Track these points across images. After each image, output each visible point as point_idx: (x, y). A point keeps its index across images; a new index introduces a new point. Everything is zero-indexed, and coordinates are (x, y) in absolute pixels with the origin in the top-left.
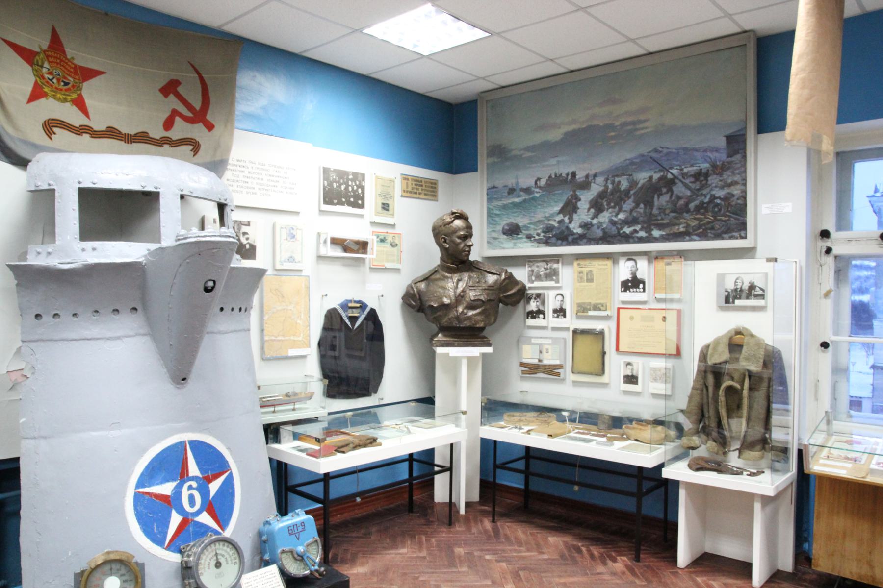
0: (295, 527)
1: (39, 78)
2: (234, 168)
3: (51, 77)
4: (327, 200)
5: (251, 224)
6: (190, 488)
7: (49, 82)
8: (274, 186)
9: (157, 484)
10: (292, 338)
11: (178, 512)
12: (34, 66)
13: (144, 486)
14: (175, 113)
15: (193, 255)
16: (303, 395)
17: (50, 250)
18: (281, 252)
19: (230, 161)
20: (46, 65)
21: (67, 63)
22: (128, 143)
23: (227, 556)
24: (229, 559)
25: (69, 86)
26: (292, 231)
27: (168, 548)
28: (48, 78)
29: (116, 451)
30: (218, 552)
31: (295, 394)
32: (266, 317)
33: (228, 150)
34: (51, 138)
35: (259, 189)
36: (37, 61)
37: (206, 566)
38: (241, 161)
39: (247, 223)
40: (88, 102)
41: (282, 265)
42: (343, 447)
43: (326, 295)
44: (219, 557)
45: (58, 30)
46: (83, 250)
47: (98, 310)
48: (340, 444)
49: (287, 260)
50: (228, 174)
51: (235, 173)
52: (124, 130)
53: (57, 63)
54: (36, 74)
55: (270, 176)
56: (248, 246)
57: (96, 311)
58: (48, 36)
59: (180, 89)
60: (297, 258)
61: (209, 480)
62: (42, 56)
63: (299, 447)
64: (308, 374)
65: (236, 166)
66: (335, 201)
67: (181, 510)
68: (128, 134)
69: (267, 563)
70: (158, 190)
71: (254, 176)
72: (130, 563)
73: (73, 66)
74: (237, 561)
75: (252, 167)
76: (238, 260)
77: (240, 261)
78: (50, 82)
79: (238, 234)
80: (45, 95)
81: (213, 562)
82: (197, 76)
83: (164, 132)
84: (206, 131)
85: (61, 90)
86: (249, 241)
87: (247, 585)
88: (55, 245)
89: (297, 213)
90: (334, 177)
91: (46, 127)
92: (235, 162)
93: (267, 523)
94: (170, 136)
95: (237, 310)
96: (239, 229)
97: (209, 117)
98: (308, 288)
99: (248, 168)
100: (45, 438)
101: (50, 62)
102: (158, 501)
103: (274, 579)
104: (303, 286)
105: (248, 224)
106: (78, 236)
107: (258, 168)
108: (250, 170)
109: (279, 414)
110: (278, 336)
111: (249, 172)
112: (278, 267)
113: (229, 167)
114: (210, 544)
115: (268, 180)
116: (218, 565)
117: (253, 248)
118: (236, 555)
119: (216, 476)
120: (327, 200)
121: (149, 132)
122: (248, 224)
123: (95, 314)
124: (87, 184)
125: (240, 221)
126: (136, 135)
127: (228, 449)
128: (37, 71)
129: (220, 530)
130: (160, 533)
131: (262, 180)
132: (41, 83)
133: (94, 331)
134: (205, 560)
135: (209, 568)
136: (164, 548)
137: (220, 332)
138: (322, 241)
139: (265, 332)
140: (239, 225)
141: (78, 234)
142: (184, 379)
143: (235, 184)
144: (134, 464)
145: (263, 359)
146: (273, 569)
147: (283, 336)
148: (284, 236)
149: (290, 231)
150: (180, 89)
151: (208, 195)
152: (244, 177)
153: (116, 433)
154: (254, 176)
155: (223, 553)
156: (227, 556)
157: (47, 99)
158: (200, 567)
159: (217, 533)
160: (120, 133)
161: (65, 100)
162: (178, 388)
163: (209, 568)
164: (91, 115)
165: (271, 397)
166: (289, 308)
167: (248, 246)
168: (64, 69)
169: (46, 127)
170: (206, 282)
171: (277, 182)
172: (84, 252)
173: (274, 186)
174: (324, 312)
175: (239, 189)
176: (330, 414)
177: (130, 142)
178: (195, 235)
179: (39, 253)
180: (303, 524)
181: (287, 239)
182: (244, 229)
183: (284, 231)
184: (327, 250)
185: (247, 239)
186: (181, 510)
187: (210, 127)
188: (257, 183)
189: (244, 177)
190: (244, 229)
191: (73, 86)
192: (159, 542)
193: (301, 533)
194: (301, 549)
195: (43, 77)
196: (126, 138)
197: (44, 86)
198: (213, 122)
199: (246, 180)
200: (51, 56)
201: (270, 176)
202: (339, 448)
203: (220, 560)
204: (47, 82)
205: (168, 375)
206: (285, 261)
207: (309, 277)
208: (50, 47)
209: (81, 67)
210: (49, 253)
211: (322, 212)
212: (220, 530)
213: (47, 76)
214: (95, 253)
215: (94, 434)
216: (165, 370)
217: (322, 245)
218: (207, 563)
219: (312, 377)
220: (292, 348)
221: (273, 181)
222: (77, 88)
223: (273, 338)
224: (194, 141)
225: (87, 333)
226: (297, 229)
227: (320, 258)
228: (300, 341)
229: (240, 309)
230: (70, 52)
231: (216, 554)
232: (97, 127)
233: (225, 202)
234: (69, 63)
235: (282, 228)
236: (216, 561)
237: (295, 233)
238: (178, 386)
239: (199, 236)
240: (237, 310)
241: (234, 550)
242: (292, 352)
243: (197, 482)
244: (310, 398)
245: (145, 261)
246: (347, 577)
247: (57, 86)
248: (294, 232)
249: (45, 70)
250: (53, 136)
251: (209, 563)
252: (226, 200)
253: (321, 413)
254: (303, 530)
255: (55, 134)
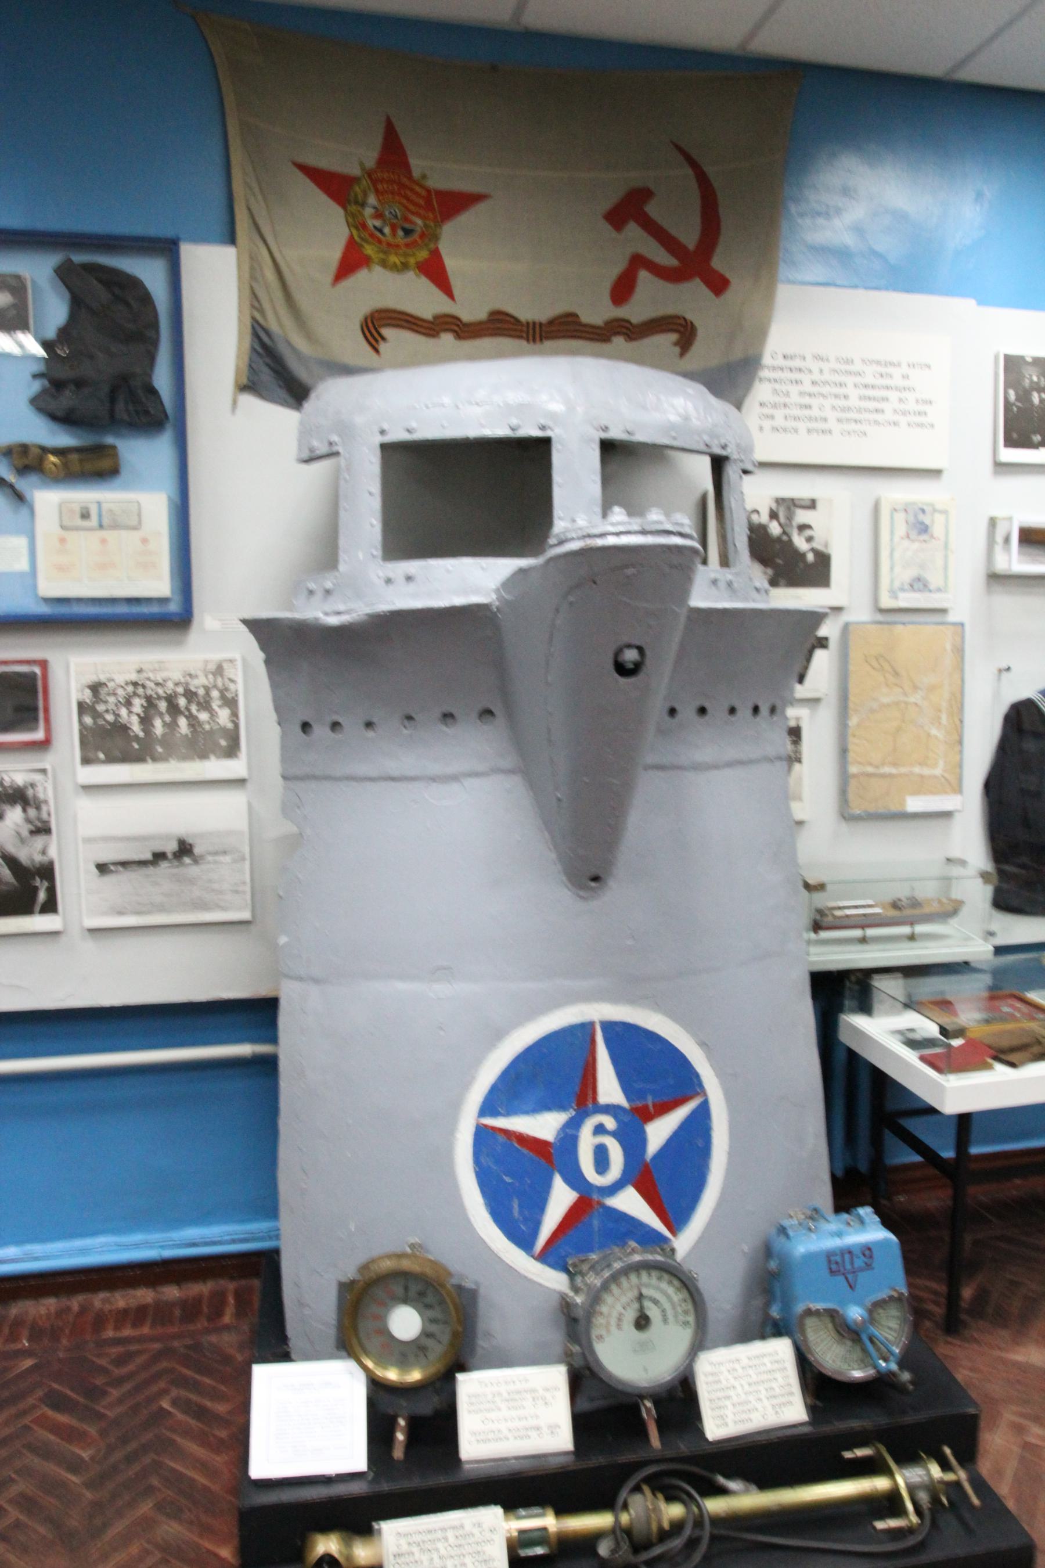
0: (847, 1257)
1: (357, 228)
2: (778, 375)
3: (378, 223)
4: (1015, 436)
5: (819, 505)
6: (600, 1129)
7: (377, 233)
8: (877, 411)
9: (526, 1112)
10: (917, 770)
11: (567, 1181)
12: (349, 208)
13: (495, 1114)
14: (638, 262)
15: (578, 586)
16: (935, 907)
17: (329, 585)
18: (892, 568)
19: (767, 360)
20: (372, 200)
21: (412, 190)
22: (534, 341)
23: (667, 1305)
24: (670, 1313)
25: (416, 236)
26: (921, 517)
27: (543, 1257)
28: (375, 227)
29: (441, 1028)
30: (645, 1291)
31: (915, 903)
32: (853, 721)
33: (761, 333)
34: (377, 351)
35: (839, 420)
36: (356, 196)
37: (613, 1321)
38: (792, 357)
39: (808, 503)
40: (451, 264)
41: (896, 598)
42: (1013, 1050)
43: (1008, 669)
44: (647, 1304)
45: (394, 120)
46: (389, 581)
47: (414, 715)
48: (1005, 1043)
49: (907, 587)
50: (761, 391)
51: (777, 386)
52: (526, 314)
53: (392, 193)
54: (350, 220)
55: (866, 386)
56: (810, 557)
57: (409, 718)
58: (378, 140)
59: (652, 209)
60: (934, 579)
61: (646, 1115)
62: (365, 183)
63: (912, 1030)
64: (956, 853)
65: (782, 369)
66: (1037, 438)
67: (575, 1179)
68: (534, 323)
69: (777, 1329)
70: (548, 433)
71: (825, 390)
72: (443, 1286)
73: (424, 193)
74: (691, 1319)
75: (821, 371)
76: (757, 590)
77: (767, 592)
78: (378, 234)
79: (788, 530)
80: (365, 262)
81: (631, 1315)
82: (690, 172)
83: (612, 307)
84: (709, 294)
85: (398, 246)
86: (815, 545)
87: (711, 1379)
88: (337, 574)
89: (936, 473)
90: (1035, 379)
91: (370, 332)
92: (780, 362)
93: (783, 1231)
94: (627, 316)
95: (745, 712)
96: (790, 518)
97: (718, 263)
98: (959, 651)
99: (810, 371)
100: (316, 981)
101: (377, 191)
102: (525, 1151)
103: (778, 1375)
104: (948, 647)
105: (812, 505)
106: (378, 552)
107: (835, 371)
108: (816, 376)
109: (874, 947)
110: (883, 764)
111: (814, 383)
112: (886, 602)
113: (764, 373)
114: (626, 1271)
115: (862, 398)
116: (642, 1322)
117: (823, 560)
118: (690, 1306)
119: (664, 1108)
120: (1015, 436)
121: (579, 313)
122: (812, 505)
123: (406, 722)
124: (398, 435)
125: (793, 500)
126: (551, 322)
127: (703, 1044)
128: (353, 215)
129: (666, 1232)
130: (526, 1220)
131: (846, 397)
132: (360, 237)
133: (406, 762)
134: (613, 1307)
135: (619, 1326)
136: (533, 1256)
137: (698, 767)
138: (999, 538)
139: (851, 756)
140: (789, 509)
141: (379, 546)
142: (596, 879)
143: (779, 414)
144: (477, 1062)
145: (844, 818)
146: (782, 1348)
147: (895, 764)
148: (901, 529)
149: (916, 516)
150: (652, 209)
151: (675, 438)
152: (801, 394)
153: (441, 989)
154: (825, 390)
155: (657, 1295)
156: (667, 1305)
157: (370, 270)
158: (599, 1321)
159: (649, 1238)
160: (517, 321)
161: (405, 267)
162: (581, 897)
163: (619, 1326)
164: (456, 292)
165: (856, 907)
166: (912, 699)
167: (810, 557)
168: (405, 202)
169: (370, 332)
170: (618, 652)
171: (885, 399)
172: (391, 587)
173: (877, 411)
174: (1003, 709)
175: (791, 424)
176: (999, 950)
177: (531, 338)
178: (580, 533)
179: (311, 592)
180: (867, 1253)
181: (908, 536)
182: (802, 516)
183: (900, 517)
184: (1010, 561)
185: (809, 539)
186: (575, 1179)
187: (718, 285)
188: (833, 407)
189: (801, 394)
190: (802, 516)
191: (422, 235)
192: (523, 1240)
193: (860, 1274)
194: (855, 1313)
195: (364, 226)
196: (531, 332)
197: (363, 243)
198: (728, 275)
199: (806, 400)
200: (382, 181)
201: (866, 386)
202: (1003, 1051)
203: (648, 1313)
204: (372, 235)
205: (559, 867)
206: (902, 590)
207: (962, 625)
208: (382, 162)
209: (440, 194)
210: (328, 592)
211: (1001, 468)
212: (666, 1232)
213: (371, 223)
214: (411, 587)
215: (401, 986)
216: (553, 856)
217: (998, 549)
218: (615, 1314)
219: (963, 863)
220: (917, 792)
221: (875, 399)
222: (431, 236)
223: (870, 769)
224: (682, 322)
225: (392, 767)
226: (935, 510)
227: (996, 579)
228: (935, 777)
229: (756, 710)
230: (417, 164)
231: (640, 1297)
232: (467, 316)
233: (723, 453)
234: (417, 189)
235: (895, 510)
236: (637, 1314)
237: (927, 522)
238: (582, 893)
239: (589, 536)
240: (745, 712)
241: (685, 1294)
242: (914, 804)
243: (616, 1117)
244: (954, 912)
245: (497, 603)
246: (975, 1404)
247: (390, 239)
248: (927, 520)
249: (368, 211)
250: (382, 347)
251: (621, 1314)
252: (724, 447)
253: (979, 950)
254: (868, 1266)
255: (383, 339)
